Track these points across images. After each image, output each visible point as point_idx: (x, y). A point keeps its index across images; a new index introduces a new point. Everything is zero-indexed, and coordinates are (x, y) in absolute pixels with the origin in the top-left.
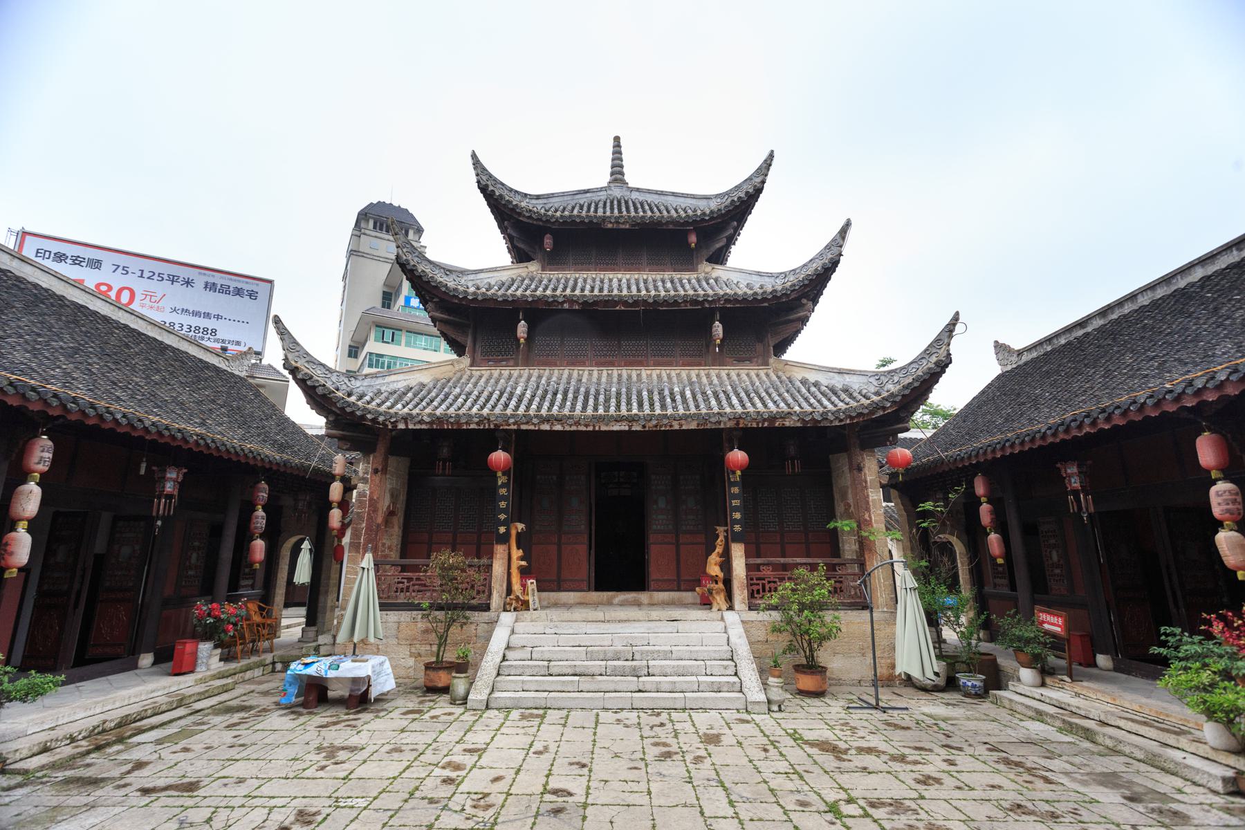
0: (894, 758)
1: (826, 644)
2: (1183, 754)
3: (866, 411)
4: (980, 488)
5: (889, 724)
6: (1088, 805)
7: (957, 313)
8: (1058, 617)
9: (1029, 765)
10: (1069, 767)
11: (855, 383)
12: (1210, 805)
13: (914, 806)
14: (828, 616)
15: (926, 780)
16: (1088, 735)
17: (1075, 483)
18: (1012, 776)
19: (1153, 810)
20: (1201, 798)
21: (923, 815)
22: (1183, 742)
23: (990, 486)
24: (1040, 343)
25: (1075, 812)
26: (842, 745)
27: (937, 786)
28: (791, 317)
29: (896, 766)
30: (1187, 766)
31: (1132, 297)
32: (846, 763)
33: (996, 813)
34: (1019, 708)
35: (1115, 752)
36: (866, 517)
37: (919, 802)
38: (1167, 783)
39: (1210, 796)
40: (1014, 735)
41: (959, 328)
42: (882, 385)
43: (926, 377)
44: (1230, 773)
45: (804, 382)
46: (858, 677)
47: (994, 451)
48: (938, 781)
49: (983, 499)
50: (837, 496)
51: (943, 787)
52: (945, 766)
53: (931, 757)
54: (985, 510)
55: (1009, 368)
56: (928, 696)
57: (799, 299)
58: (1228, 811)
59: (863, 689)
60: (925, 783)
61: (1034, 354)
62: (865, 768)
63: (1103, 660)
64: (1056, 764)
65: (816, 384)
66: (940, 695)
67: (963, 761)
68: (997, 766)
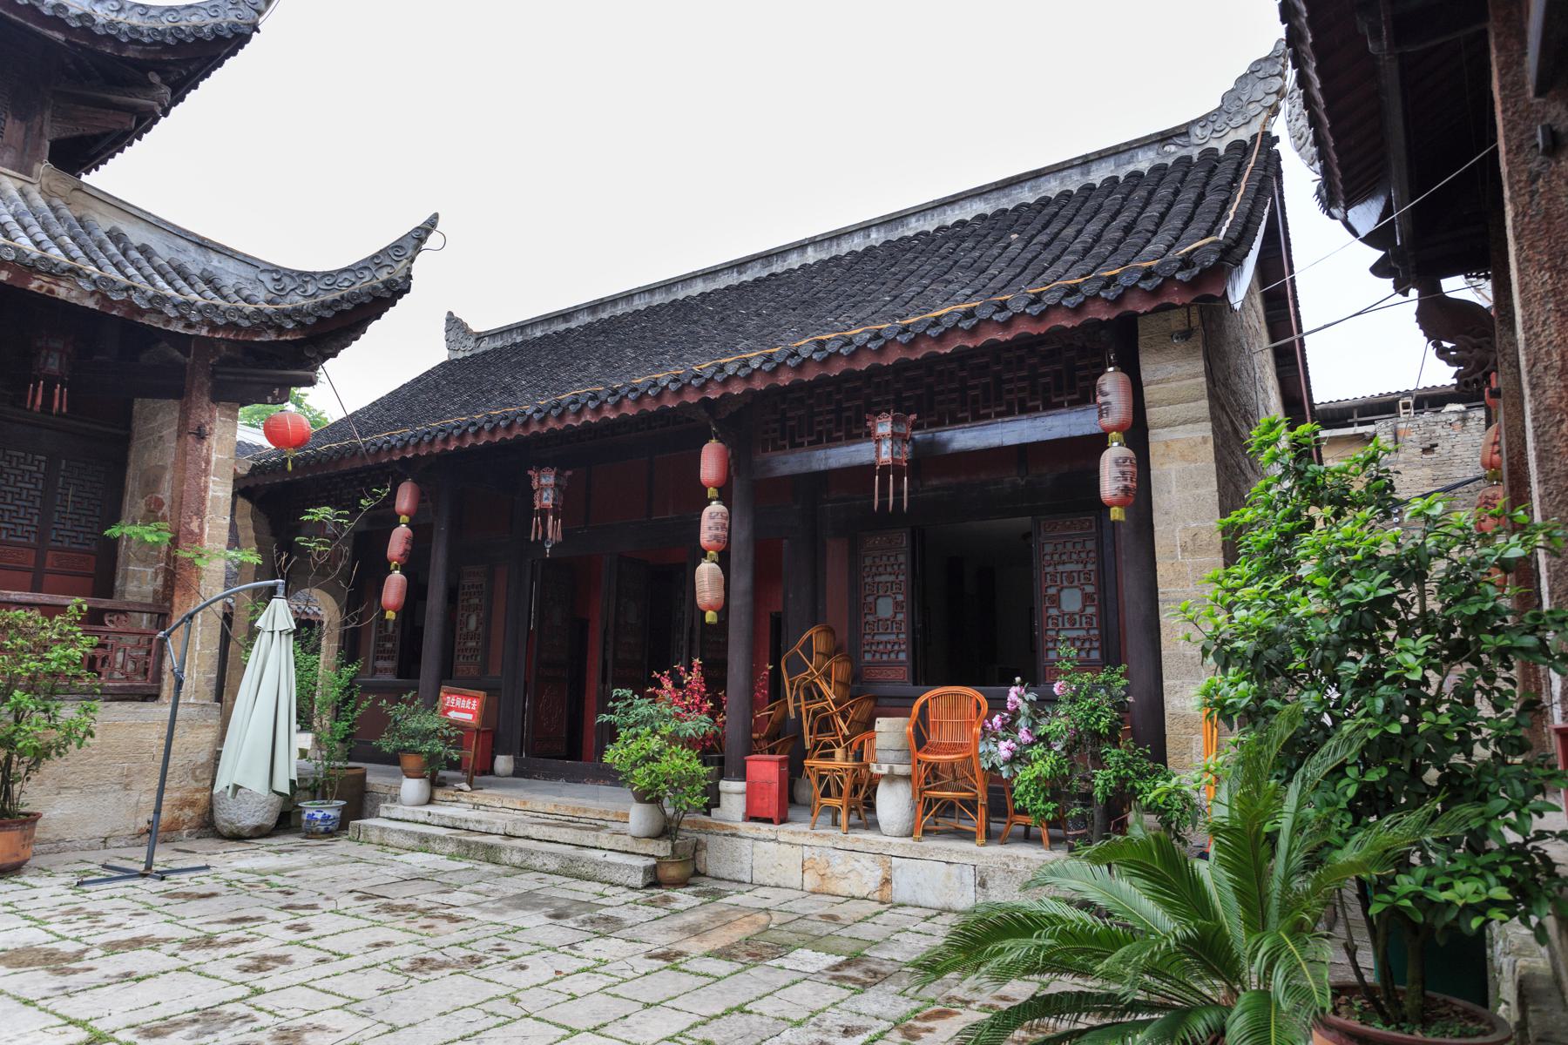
0: (189, 945)
1: (51, 767)
2: (603, 853)
3: (246, 323)
4: (405, 500)
5: (174, 896)
6: (512, 936)
7: (436, 216)
8: (473, 697)
9: (422, 906)
10: (473, 897)
11: (230, 273)
12: (635, 902)
13: (242, 1009)
14: (68, 711)
15: (261, 964)
16: (490, 854)
17: (546, 499)
18: (402, 925)
19: (584, 922)
20: (624, 898)
21: (264, 1019)
22: (604, 839)
23: (421, 499)
24: (509, 330)
25: (499, 949)
26: (69, 947)
27: (283, 967)
28: (115, 98)
29: (196, 956)
30: (609, 865)
31: (628, 296)
32: (80, 977)
33: (390, 980)
34: (395, 839)
35: (523, 868)
36: (194, 526)
37: (253, 1000)
38: (587, 891)
39: (631, 893)
40: (390, 873)
41: (433, 240)
42: (281, 293)
43: (366, 300)
44: (652, 861)
45: (117, 237)
46: (102, 831)
47: (446, 441)
48: (283, 960)
49: (404, 518)
50: (132, 485)
51: (293, 966)
52: (292, 936)
53: (263, 928)
54: (398, 541)
55: (460, 355)
56: (242, 846)
57: (142, 66)
58: (652, 903)
59: (111, 852)
60: (259, 969)
61: (498, 344)
62: (128, 975)
63: (503, 763)
64: (456, 897)
65: (144, 250)
66: (265, 841)
67: (320, 922)
68: (376, 917)
